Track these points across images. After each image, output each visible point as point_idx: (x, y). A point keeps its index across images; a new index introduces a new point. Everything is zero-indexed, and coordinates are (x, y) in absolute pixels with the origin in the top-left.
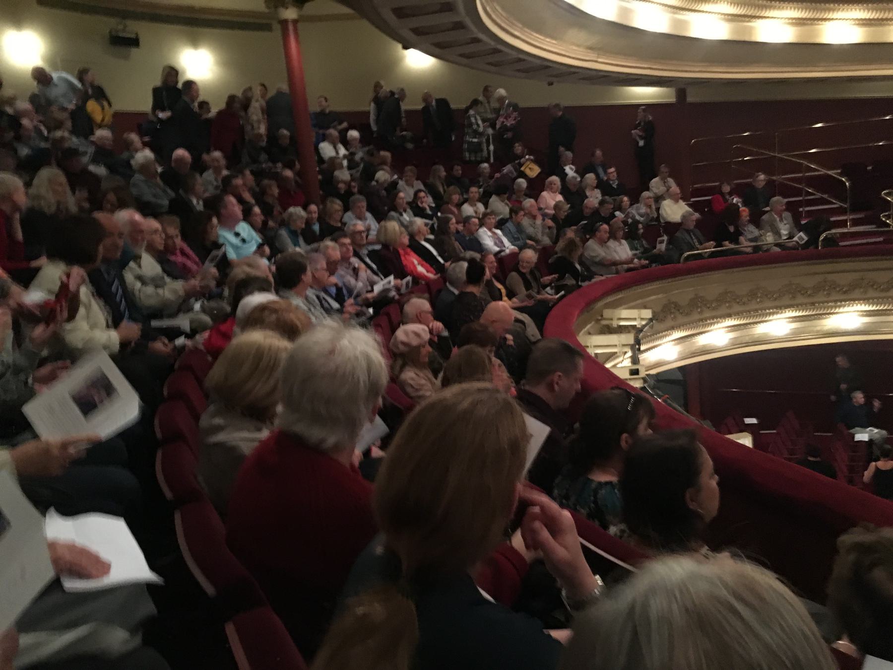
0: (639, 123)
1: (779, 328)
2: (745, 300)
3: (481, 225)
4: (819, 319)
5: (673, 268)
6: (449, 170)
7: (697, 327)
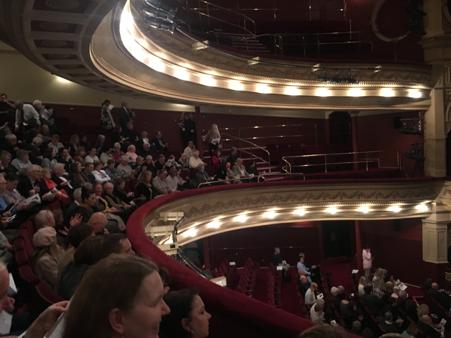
0: (182, 120)
1: (242, 219)
2: (227, 206)
3: (95, 169)
4: (259, 214)
5: (198, 191)
6: (81, 137)
7: (206, 220)
